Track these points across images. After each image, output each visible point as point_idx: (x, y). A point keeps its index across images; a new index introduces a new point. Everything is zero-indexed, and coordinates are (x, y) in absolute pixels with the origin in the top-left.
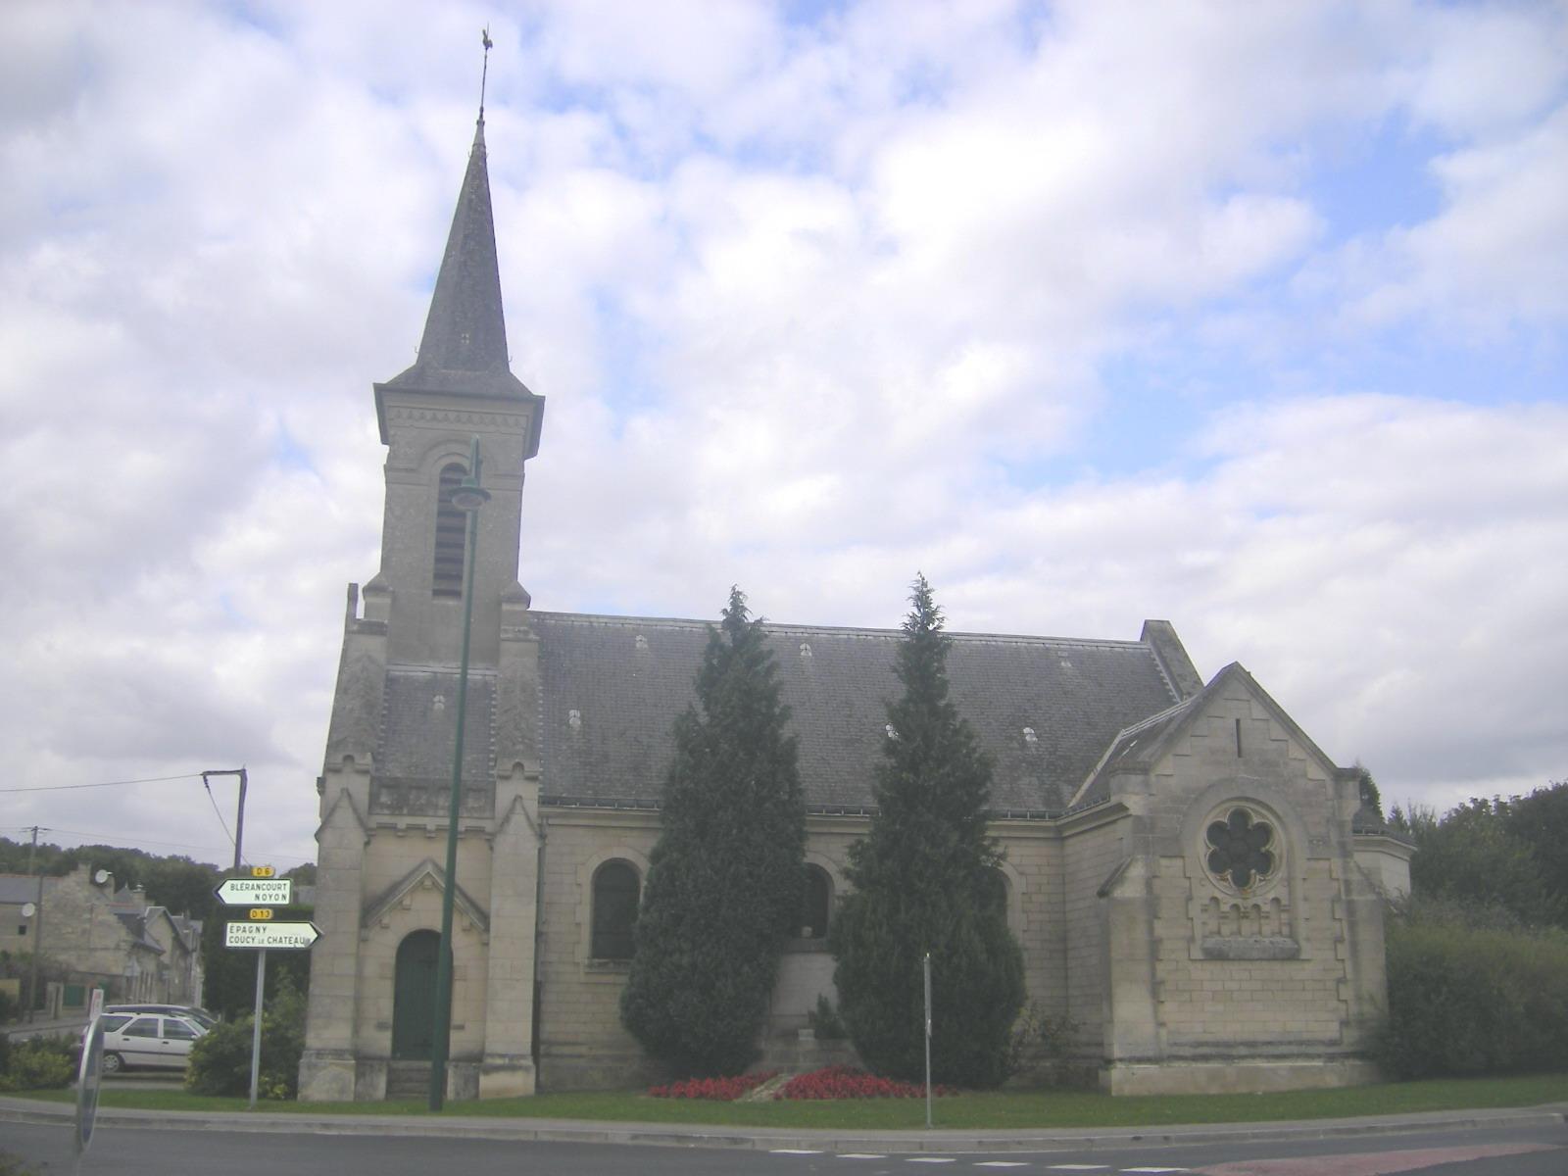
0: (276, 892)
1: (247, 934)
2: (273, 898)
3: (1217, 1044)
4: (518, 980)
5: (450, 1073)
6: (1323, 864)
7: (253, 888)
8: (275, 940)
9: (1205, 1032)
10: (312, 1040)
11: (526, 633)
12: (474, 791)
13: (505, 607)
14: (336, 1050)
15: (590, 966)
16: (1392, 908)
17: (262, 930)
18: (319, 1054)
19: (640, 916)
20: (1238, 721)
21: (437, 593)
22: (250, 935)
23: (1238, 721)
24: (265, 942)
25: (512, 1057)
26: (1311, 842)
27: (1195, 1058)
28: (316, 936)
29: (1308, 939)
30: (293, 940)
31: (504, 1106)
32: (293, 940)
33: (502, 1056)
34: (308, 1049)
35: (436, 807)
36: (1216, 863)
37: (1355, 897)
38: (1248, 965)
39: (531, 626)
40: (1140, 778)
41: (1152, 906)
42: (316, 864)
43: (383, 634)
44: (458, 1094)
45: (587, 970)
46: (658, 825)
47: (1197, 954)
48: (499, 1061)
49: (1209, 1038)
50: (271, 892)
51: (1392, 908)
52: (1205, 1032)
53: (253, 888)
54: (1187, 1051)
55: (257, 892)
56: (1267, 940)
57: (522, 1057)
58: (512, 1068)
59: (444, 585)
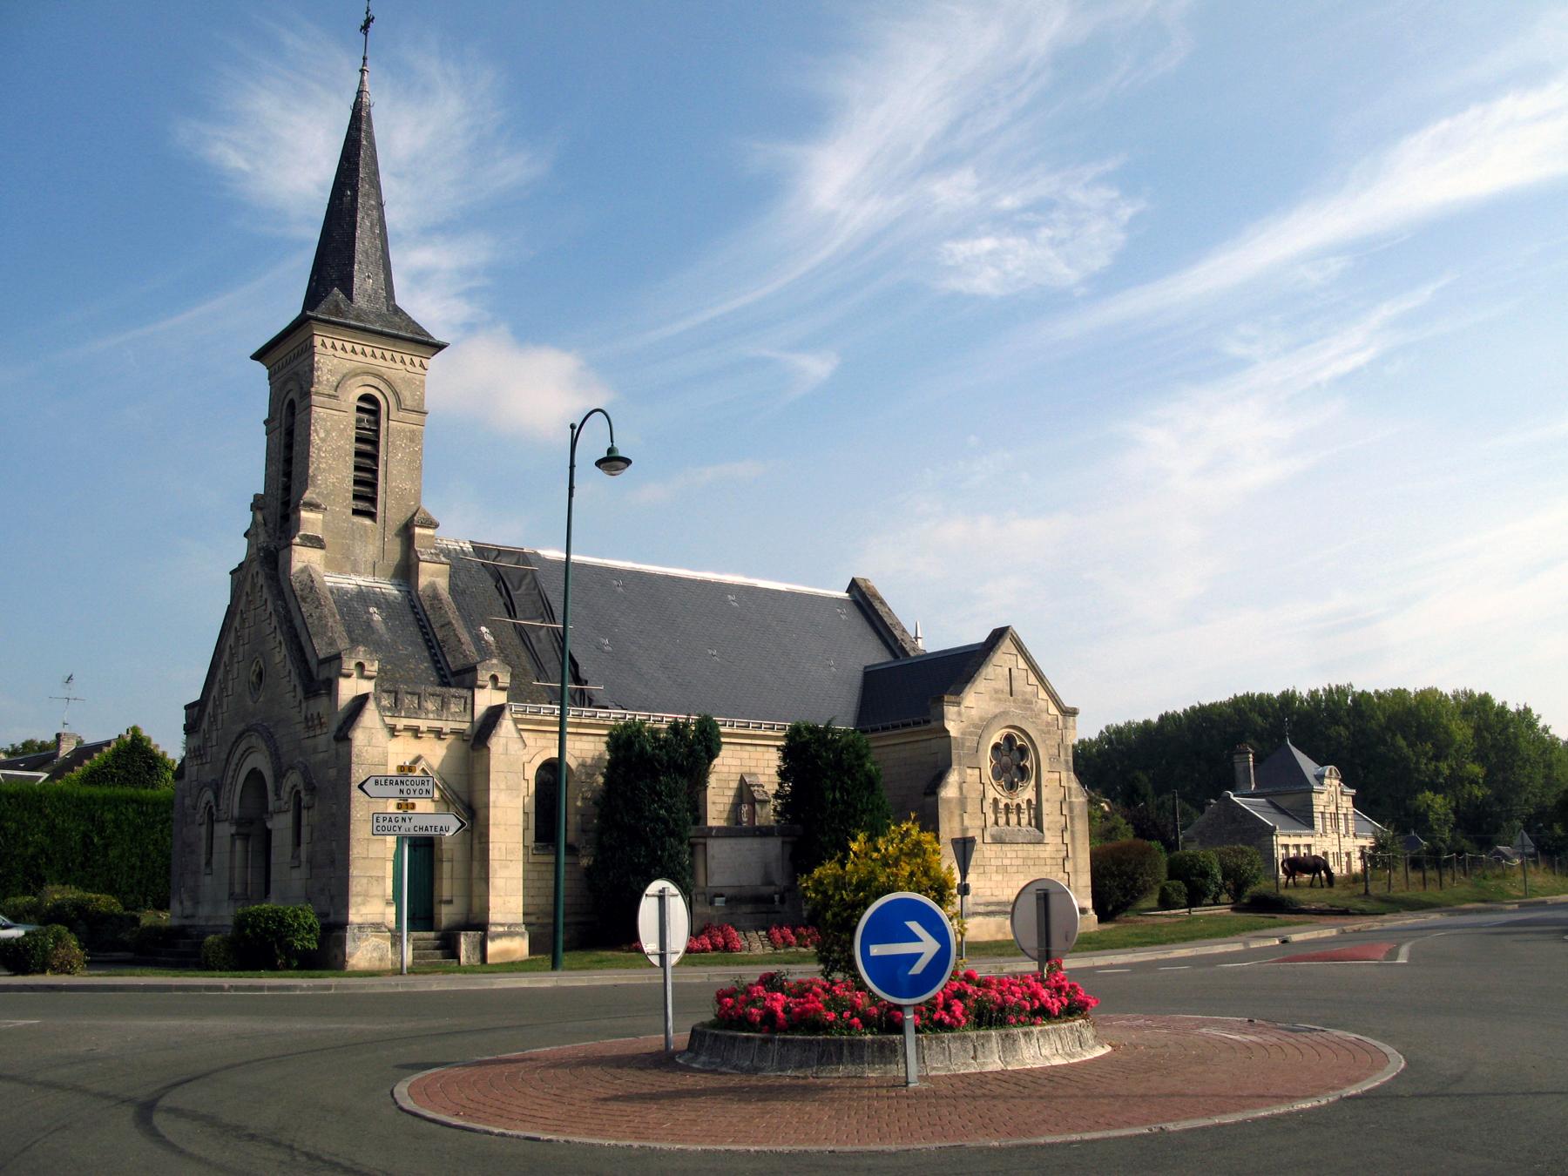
0: (420, 787)
1: (394, 823)
2: (417, 792)
3: (998, 904)
4: (511, 861)
5: (462, 940)
6: (1057, 775)
7: (397, 783)
8: (421, 829)
9: (992, 895)
10: (354, 916)
11: (437, 555)
12: (456, 697)
13: (418, 530)
14: (373, 924)
15: (536, 848)
16: (656, 764)
17: (407, 820)
18: (361, 927)
19: (1124, 840)
20: (1010, 669)
21: (356, 512)
22: (396, 824)
23: (1010, 669)
24: (412, 830)
25: (510, 926)
26: (1050, 759)
27: (988, 914)
28: (460, 824)
29: (1048, 829)
30: (438, 829)
31: (512, 967)
32: (438, 829)
33: (502, 925)
34: (352, 924)
35: (427, 712)
36: (997, 774)
37: (1073, 799)
38: (1015, 847)
39: (442, 551)
40: (956, 709)
41: (962, 801)
42: (171, 744)
43: (322, 547)
44: (468, 957)
45: (534, 852)
46: (723, 740)
47: (988, 839)
48: (500, 929)
49: (994, 899)
50: (415, 787)
51: (656, 764)
52: (992, 895)
53: (397, 783)
54: (981, 909)
55: (402, 787)
56: (1024, 829)
57: (517, 925)
58: (510, 934)
59: (362, 505)
